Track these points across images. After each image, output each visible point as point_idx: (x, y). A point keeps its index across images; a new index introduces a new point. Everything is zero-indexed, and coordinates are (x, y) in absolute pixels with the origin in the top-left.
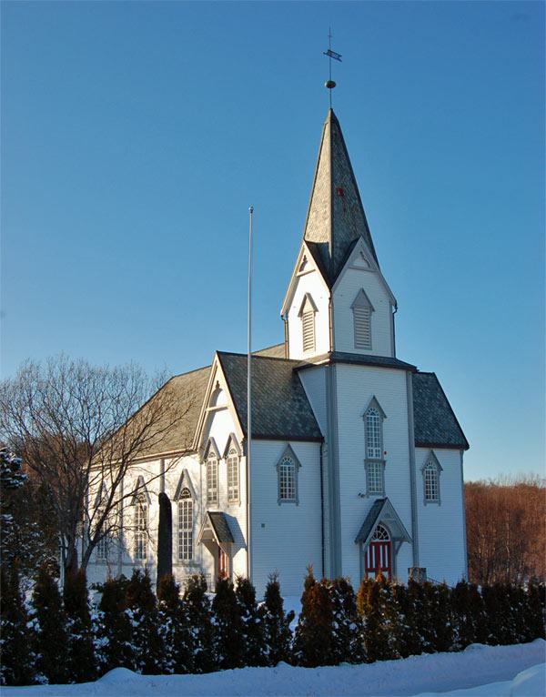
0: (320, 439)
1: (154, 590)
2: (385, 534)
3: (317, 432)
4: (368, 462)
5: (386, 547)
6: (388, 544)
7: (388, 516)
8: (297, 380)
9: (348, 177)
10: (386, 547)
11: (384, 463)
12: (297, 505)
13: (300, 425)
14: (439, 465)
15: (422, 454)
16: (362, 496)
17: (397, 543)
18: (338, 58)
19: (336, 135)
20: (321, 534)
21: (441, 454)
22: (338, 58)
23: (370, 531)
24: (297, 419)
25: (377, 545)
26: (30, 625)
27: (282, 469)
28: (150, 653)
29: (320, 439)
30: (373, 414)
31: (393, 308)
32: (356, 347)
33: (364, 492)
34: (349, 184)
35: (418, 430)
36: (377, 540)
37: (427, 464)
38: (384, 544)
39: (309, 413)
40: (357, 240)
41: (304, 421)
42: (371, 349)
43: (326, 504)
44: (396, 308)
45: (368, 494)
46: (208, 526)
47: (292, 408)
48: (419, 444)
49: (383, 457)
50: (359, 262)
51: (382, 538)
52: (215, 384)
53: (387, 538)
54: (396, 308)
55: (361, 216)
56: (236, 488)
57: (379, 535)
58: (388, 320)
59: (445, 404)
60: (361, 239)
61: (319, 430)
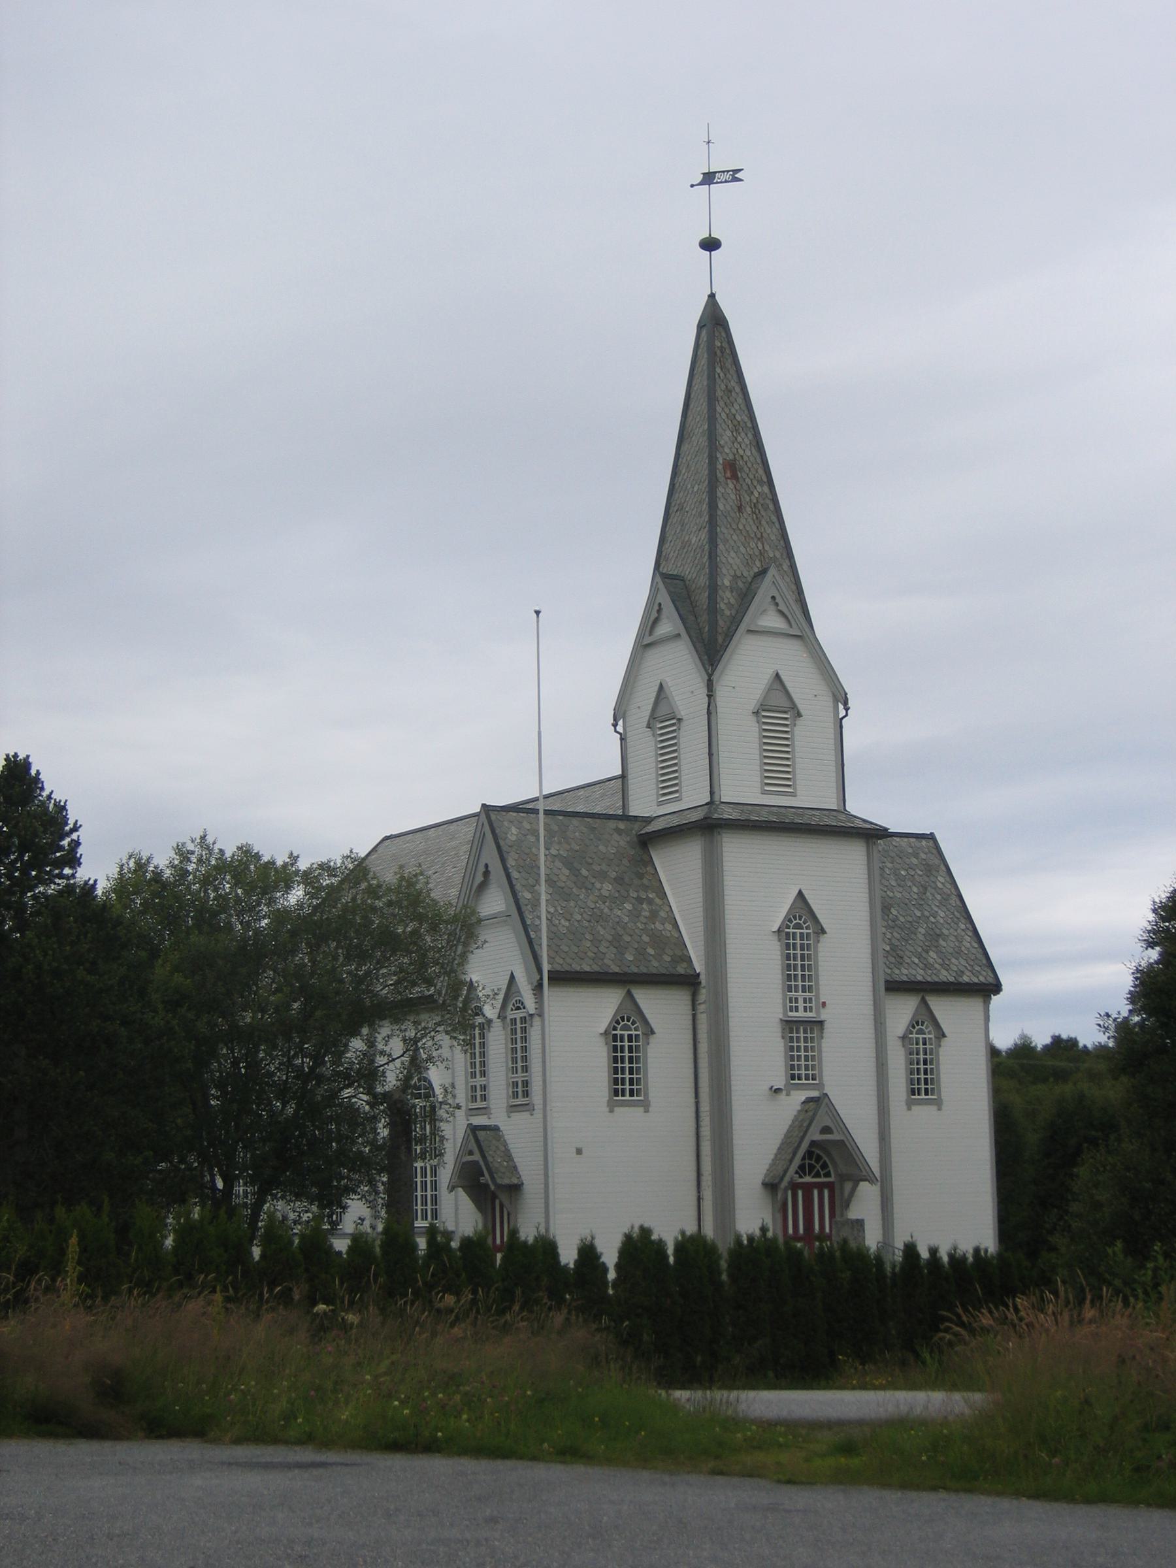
0: (690, 982)
1: (724, 1277)
2: (824, 1166)
3: (685, 965)
4: (790, 1025)
5: (826, 1192)
6: (830, 1186)
7: (826, 1130)
8: (645, 857)
9: (746, 439)
10: (826, 1192)
11: (821, 1023)
12: (647, 1111)
13: (651, 951)
14: (645, 1022)
15: (902, 1011)
16: (778, 1091)
17: (848, 1186)
18: (734, 176)
19: (722, 349)
20: (694, 1168)
21: (945, 1009)
22: (734, 176)
23: (791, 1161)
24: (646, 938)
25: (808, 1188)
26: (343, 1341)
27: (615, 1038)
28: (398, 1399)
29: (690, 982)
30: (798, 926)
31: (841, 707)
32: (765, 793)
33: (780, 1083)
34: (749, 453)
35: (895, 955)
36: (808, 1179)
37: (915, 1023)
38: (821, 1187)
39: (669, 927)
40: (763, 572)
41: (659, 941)
42: (793, 794)
43: (705, 1107)
44: (847, 709)
45: (790, 1088)
46: (471, 1153)
47: (635, 915)
48: (895, 987)
49: (818, 1012)
50: (772, 621)
51: (818, 1175)
52: (481, 869)
53: (828, 1175)
54: (847, 709)
55: (774, 518)
56: (473, 1082)
57: (812, 1167)
58: (831, 733)
59: (954, 901)
60: (772, 571)
61: (689, 960)
